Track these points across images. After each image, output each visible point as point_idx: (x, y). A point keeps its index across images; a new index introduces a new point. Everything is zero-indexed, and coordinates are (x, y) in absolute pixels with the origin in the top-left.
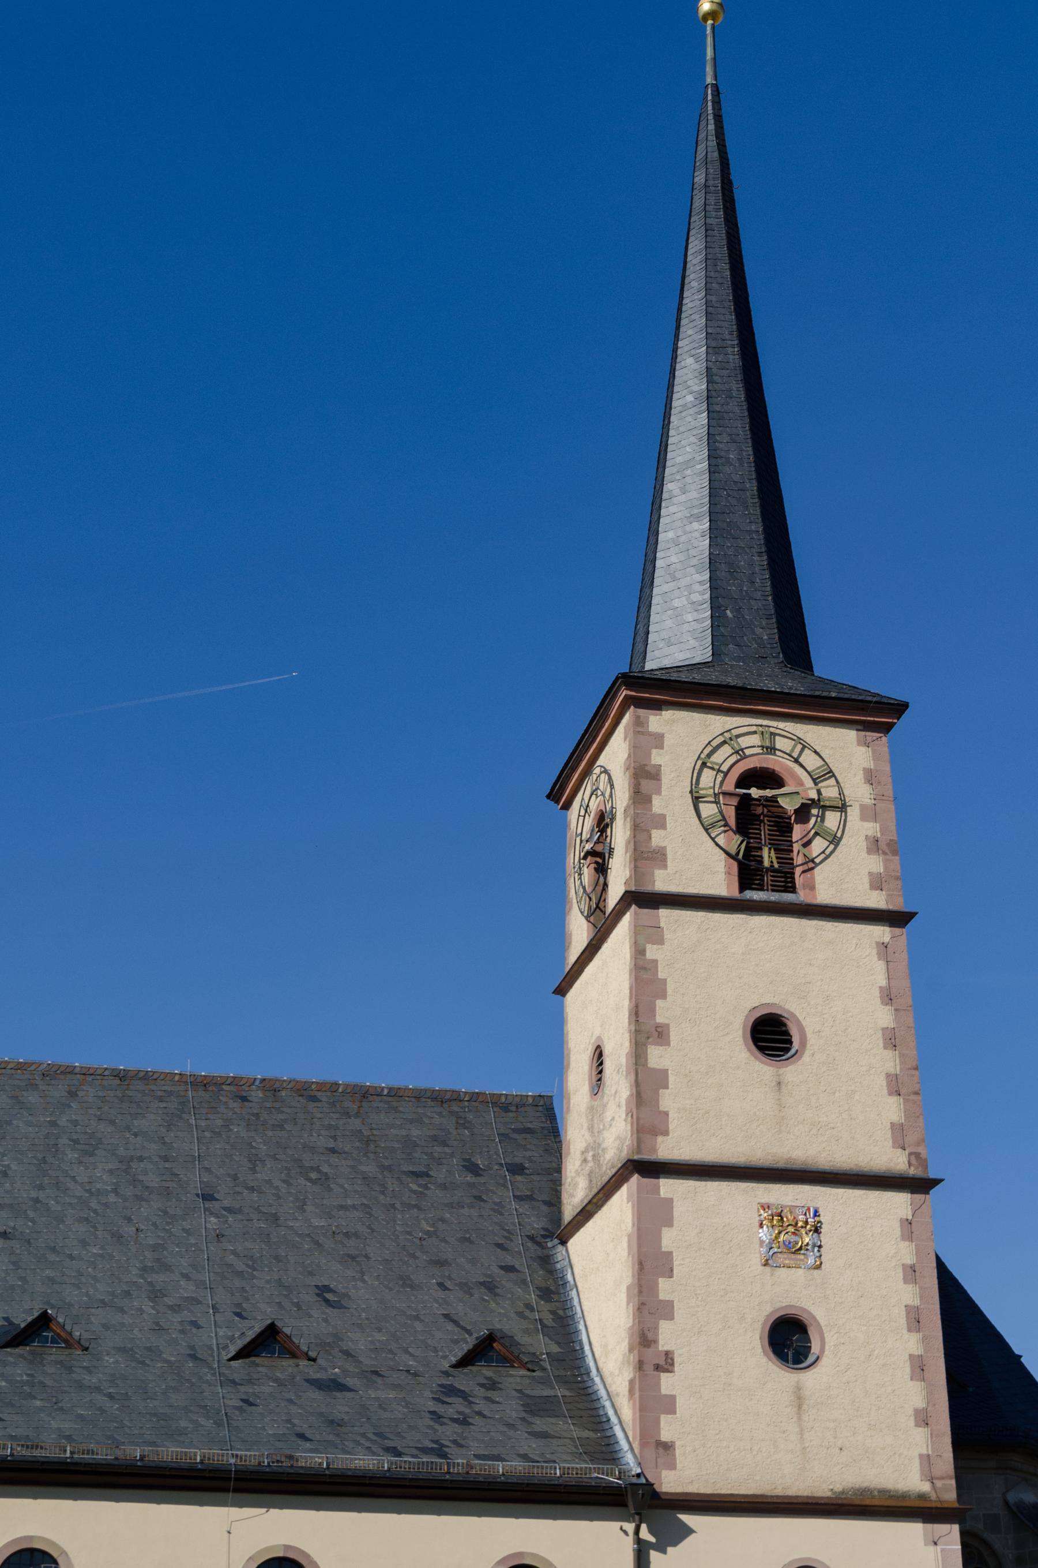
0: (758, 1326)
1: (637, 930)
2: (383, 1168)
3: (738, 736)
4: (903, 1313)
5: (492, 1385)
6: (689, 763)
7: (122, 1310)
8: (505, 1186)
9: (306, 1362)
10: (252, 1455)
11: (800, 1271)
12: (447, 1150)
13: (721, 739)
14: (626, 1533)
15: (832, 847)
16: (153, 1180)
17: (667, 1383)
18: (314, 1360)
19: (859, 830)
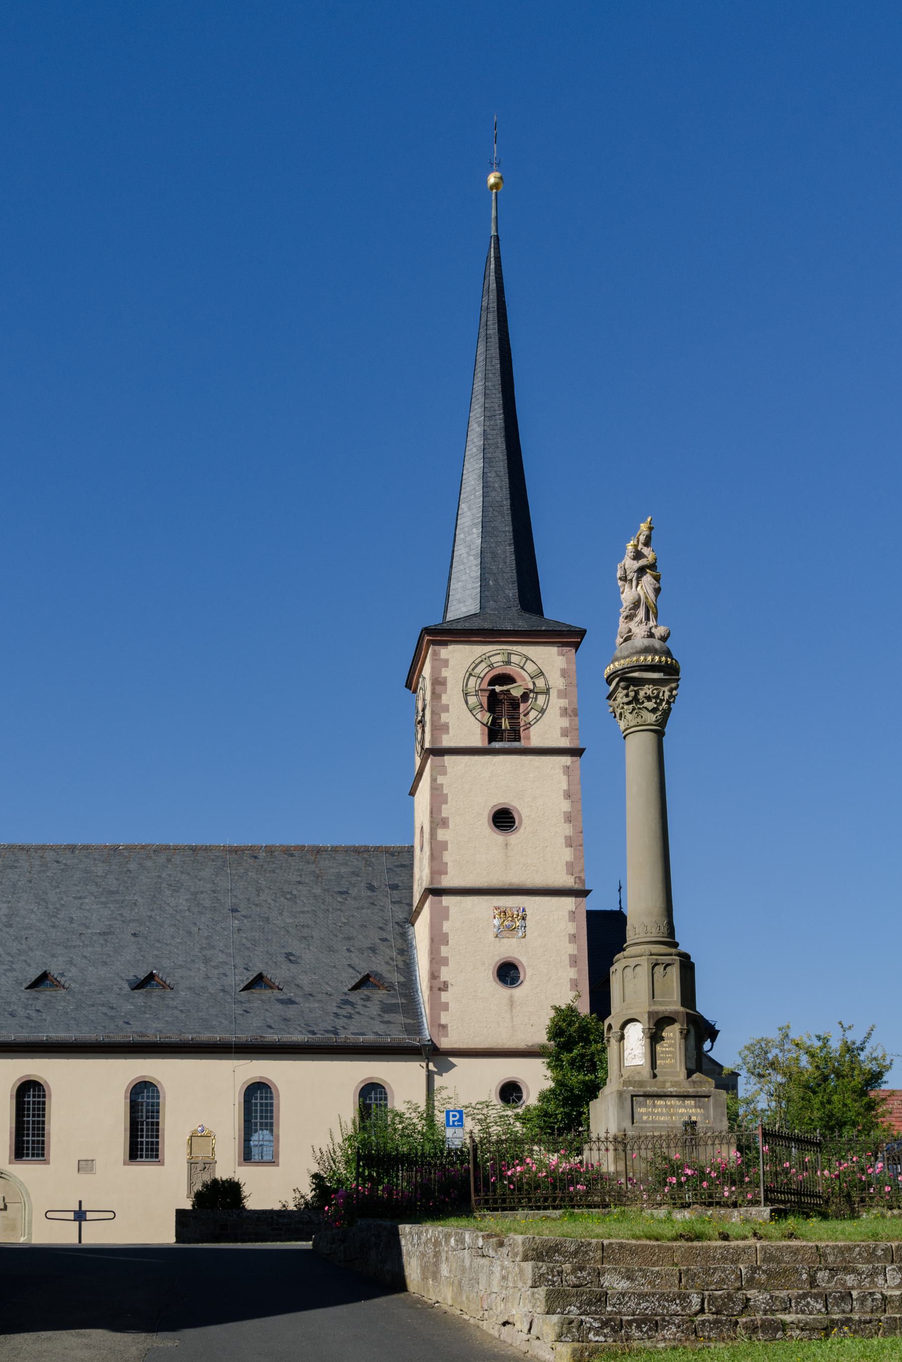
0: (492, 967)
3: (489, 657)
5: (368, 999)
6: (462, 674)
7: (190, 970)
10: (243, 1037)
11: (514, 940)
13: (480, 659)
16: (207, 903)
17: (444, 997)
19: (556, 703)
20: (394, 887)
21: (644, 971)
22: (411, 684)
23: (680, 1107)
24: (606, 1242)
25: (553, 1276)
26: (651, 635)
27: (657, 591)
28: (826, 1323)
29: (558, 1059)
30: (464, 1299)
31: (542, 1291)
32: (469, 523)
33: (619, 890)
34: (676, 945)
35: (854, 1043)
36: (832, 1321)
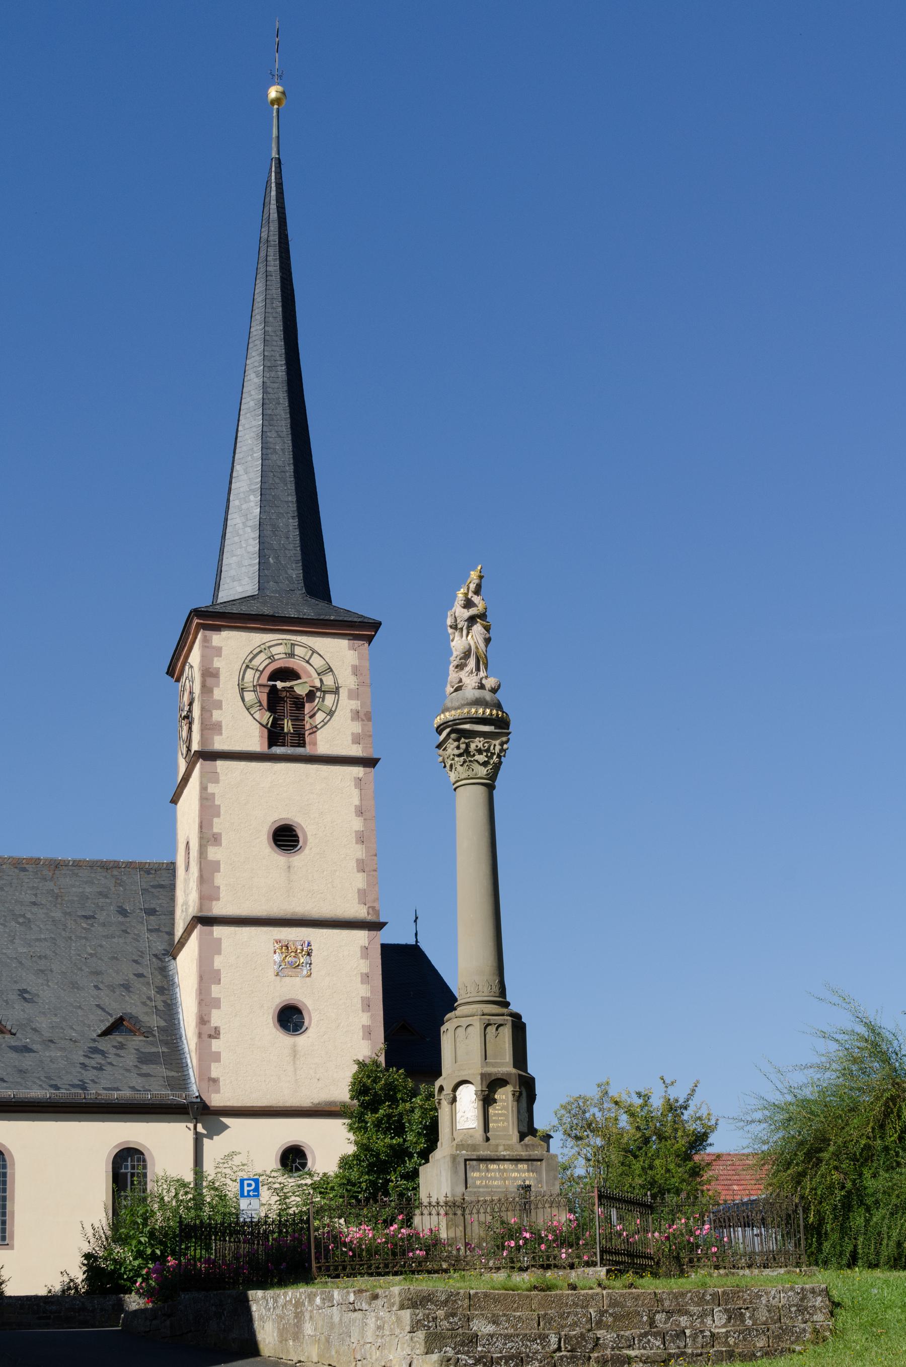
1: (202, 775)
2: (65, 913)
3: (269, 647)
4: (360, 1002)
5: (121, 1046)
6: (237, 666)
8: (142, 923)
9: (10, 1036)
11: (298, 979)
12: (108, 900)
13: (258, 650)
14: (189, 1129)
15: (329, 717)
17: (216, 1045)
18: (14, 1034)
19: (346, 705)
20: (151, 912)
21: (476, 1031)
22: (174, 670)
23: (513, 1171)
24: (472, 1292)
25: (429, 1322)
26: (482, 687)
27: (488, 641)
28: (665, 1356)
29: (361, 1119)
30: (333, 1353)
31: (421, 1335)
32: (246, 488)
33: (417, 918)
34: (506, 1005)
35: (677, 1101)
36: (669, 1354)
